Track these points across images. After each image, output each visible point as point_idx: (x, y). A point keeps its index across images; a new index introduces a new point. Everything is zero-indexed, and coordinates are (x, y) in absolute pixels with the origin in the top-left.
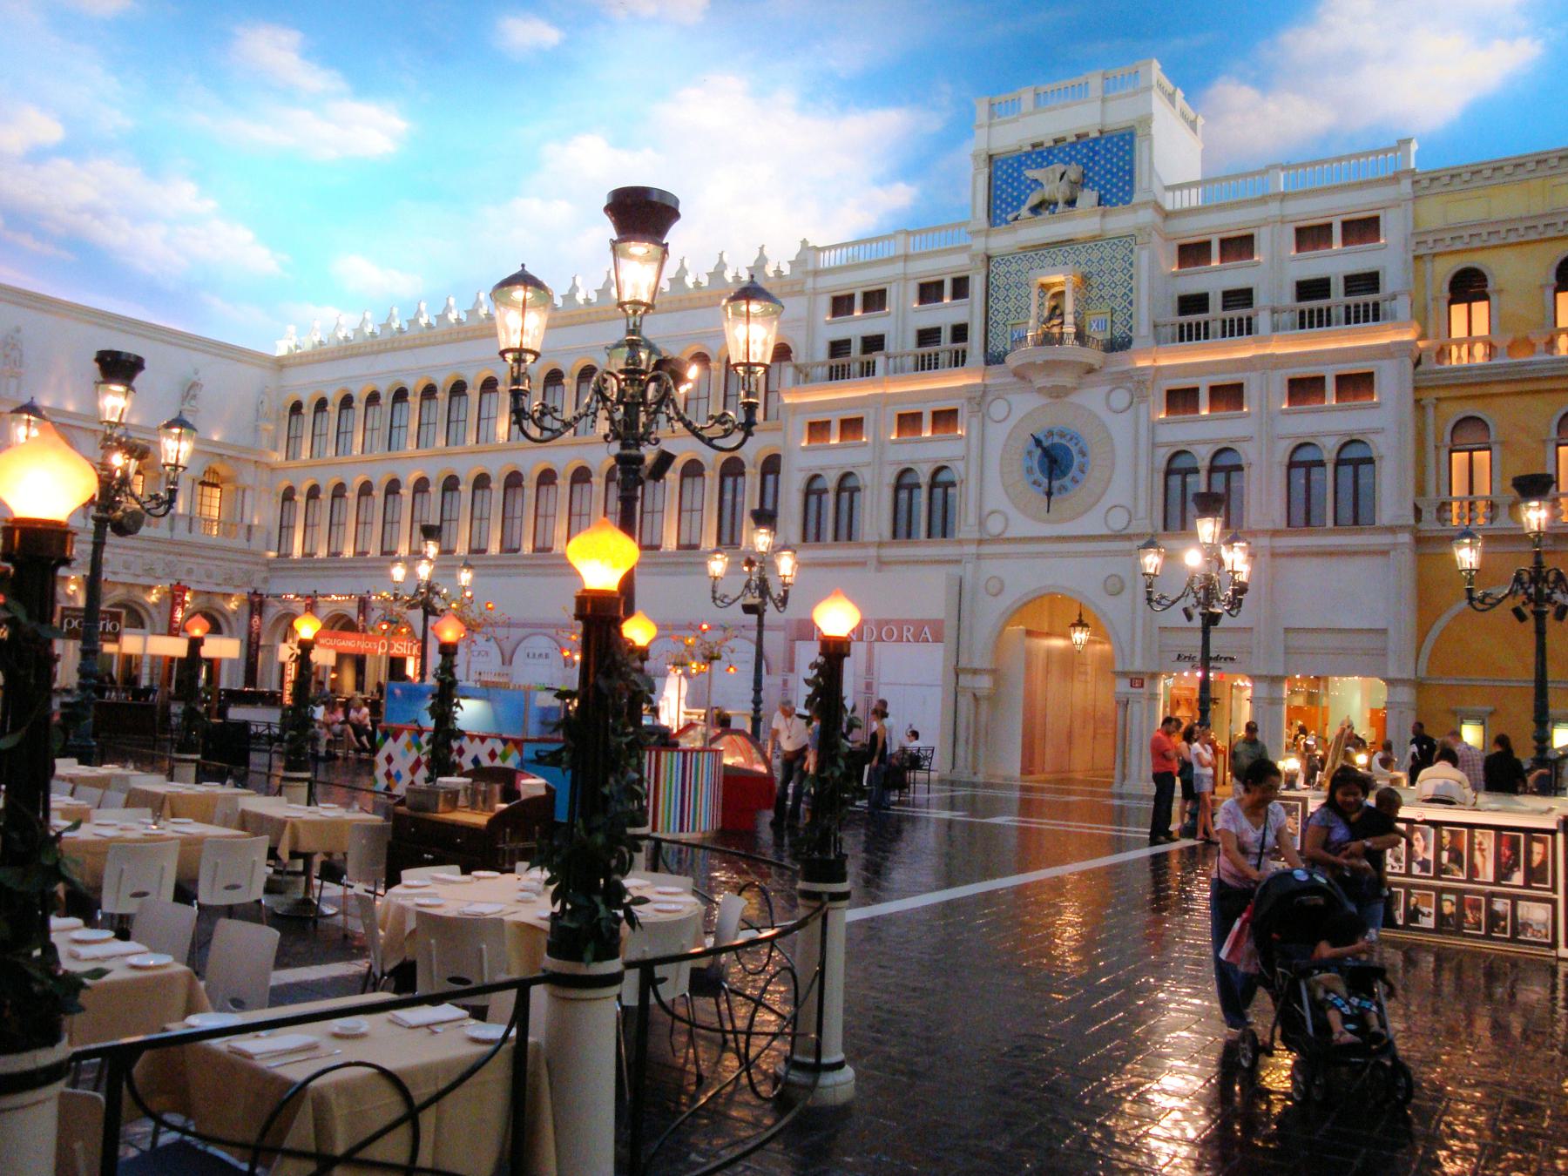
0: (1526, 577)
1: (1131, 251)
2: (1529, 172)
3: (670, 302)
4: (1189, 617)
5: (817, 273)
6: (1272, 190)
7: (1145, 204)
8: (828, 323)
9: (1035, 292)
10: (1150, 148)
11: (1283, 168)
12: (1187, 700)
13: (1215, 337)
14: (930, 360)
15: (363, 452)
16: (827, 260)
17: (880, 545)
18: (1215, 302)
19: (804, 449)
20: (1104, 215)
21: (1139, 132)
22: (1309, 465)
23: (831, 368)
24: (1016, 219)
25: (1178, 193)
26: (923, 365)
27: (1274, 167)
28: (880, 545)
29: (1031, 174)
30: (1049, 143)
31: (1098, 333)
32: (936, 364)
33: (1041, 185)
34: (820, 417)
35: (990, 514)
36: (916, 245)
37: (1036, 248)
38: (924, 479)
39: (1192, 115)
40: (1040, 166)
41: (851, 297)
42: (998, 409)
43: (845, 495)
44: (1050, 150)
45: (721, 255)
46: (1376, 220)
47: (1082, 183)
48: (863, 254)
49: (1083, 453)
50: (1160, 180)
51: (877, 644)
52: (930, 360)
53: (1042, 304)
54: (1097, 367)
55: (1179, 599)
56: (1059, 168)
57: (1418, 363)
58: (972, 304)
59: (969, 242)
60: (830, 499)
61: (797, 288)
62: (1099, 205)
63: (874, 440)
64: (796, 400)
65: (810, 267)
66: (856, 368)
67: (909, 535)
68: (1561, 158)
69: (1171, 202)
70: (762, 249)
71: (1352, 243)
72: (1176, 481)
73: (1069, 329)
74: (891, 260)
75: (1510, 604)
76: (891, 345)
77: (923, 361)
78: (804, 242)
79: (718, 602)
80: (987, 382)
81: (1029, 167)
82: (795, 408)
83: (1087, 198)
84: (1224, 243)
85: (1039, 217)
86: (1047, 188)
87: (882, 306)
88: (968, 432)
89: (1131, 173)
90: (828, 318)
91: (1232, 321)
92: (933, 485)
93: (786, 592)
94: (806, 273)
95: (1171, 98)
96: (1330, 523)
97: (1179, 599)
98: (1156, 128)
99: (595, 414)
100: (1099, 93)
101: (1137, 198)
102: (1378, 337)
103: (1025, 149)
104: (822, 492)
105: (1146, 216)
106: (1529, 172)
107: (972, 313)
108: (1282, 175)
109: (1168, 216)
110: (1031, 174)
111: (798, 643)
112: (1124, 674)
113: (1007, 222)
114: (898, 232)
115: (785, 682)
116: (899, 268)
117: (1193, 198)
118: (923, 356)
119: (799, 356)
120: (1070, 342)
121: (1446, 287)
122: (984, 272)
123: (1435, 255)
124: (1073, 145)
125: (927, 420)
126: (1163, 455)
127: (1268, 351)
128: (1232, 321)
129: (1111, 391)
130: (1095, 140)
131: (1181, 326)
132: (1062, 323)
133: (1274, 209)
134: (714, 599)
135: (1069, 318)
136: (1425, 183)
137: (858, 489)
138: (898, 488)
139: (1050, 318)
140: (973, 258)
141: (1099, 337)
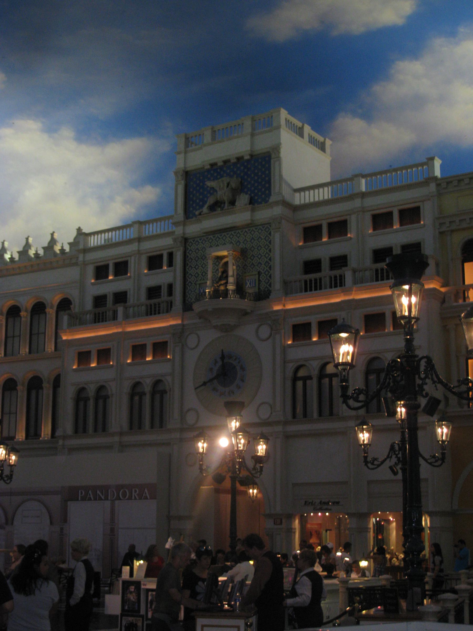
0: (397, 447)
1: (270, 234)
2: (467, 184)
3: (19, 268)
4: (395, 473)
5: (86, 250)
6: (356, 191)
7: (277, 203)
8: (93, 284)
9: (210, 264)
10: (280, 165)
11: (364, 176)
12: (316, 531)
13: (326, 288)
14: (99, 316)
15: (5, 355)
16: (94, 241)
17: (121, 434)
18: (325, 265)
19: (75, 370)
20: (253, 210)
21: (273, 156)
22: (305, 379)
23: (95, 314)
24: (200, 214)
25: (302, 194)
26: (151, 311)
27: (357, 176)
28: (121, 434)
29: (209, 184)
30: (220, 164)
31: (250, 289)
32: (159, 310)
33: (216, 191)
34: (85, 349)
35: (188, 410)
36: (150, 230)
37: (214, 232)
38: (147, 389)
39: (321, 139)
40: (216, 178)
41: (107, 266)
42: (192, 341)
43: (158, 397)
44: (221, 168)
45: (27, 239)
46: (418, 208)
47: (236, 192)
48: (115, 237)
49: (243, 369)
50: (289, 185)
51: (117, 502)
52: (155, 308)
53: (218, 270)
54: (249, 311)
55: (385, 460)
56: (226, 180)
57: (443, 301)
58: (175, 270)
59: (174, 230)
60: (91, 403)
61: (74, 261)
62: (250, 204)
63: (117, 363)
64: (70, 338)
65: (81, 247)
66: (110, 314)
67: (140, 428)
68: (471, 179)
69: (298, 199)
70: (52, 234)
71: (407, 224)
72: (372, 377)
73: (231, 287)
74: (130, 241)
75: (388, 463)
76: (131, 300)
77: (151, 308)
78: (79, 230)
79: (370, 465)
80: (186, 322)
81: (209, 179)
82: (69, 342)
83: (243, 199)
84: (330, 225)
85: (214, 213)
86: (219, 193)
87: (345, 232)
88: (174, 357)
89: (269, 182)
90: (93, 281)
91: (336, 277)
92: (153, 394)
93: (12, 471)
94: (80, 251)
95: (300, 132)
96: (315, 415)
97: (385, 460)
98: (284, 153)
99: (391, 457)
100: (250, 130)
101: (273, 199)
102: (152, 324)
103: (206, 168)
104: (142, 394)
105: (277, 211)
106: (467, 184)
107: (175, 278)
108: (363, 181)
109: (296, 209)
110: (209, 184)
111: (69, 503)
112: (269, 516)
113: (196, 216)
114: (135, 223)
115: (62, 529)
116: (134, 247)
117: (325, 194)
118: (151, 305)
119: (76, 308)
120: (231, 296)
121: (459, 252)
122: (182, 249)
123: (452, 231)
124: (235, 164)
125: (149, 349)
126: (291, 367)
127: (351, 297)
128: (311, 281)
129: (261, 325)
130: (248, 161)
131: (306, 282)
132: (227, 283)
133: (357, 203)
134: (366, 462)
135: (231, 280)
136: (444, 185)
137: (165, 392)
138: (132, 396)
139: (220, 279)
140: (175, 240)
141: (251, 291)
